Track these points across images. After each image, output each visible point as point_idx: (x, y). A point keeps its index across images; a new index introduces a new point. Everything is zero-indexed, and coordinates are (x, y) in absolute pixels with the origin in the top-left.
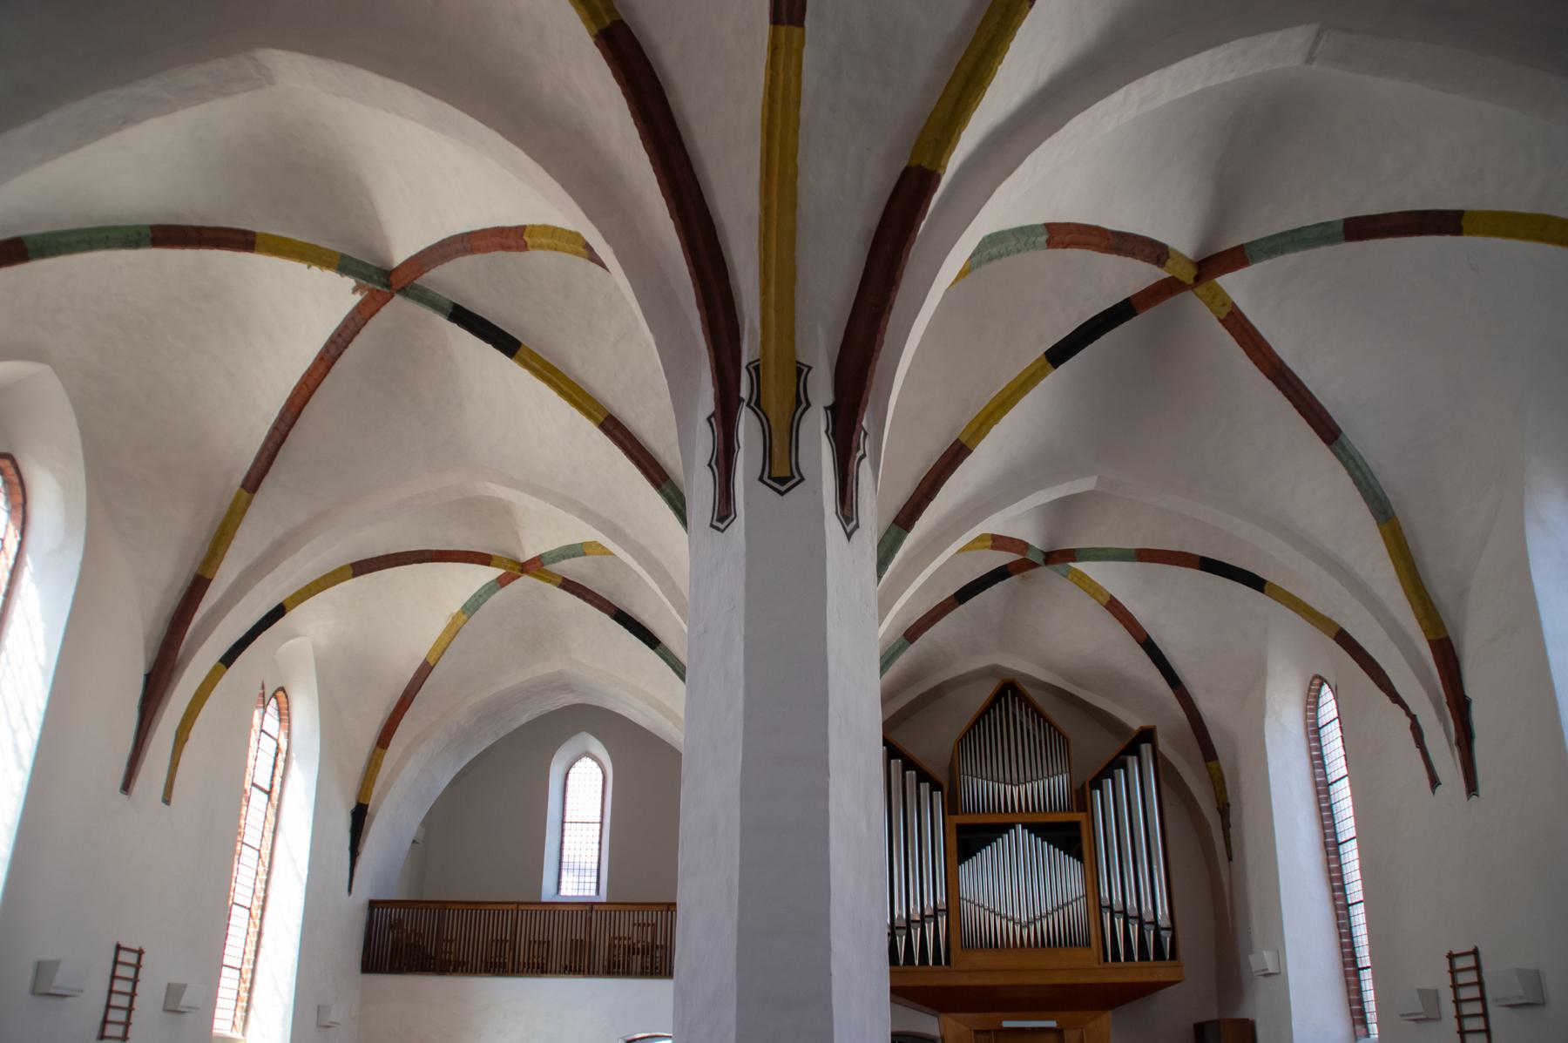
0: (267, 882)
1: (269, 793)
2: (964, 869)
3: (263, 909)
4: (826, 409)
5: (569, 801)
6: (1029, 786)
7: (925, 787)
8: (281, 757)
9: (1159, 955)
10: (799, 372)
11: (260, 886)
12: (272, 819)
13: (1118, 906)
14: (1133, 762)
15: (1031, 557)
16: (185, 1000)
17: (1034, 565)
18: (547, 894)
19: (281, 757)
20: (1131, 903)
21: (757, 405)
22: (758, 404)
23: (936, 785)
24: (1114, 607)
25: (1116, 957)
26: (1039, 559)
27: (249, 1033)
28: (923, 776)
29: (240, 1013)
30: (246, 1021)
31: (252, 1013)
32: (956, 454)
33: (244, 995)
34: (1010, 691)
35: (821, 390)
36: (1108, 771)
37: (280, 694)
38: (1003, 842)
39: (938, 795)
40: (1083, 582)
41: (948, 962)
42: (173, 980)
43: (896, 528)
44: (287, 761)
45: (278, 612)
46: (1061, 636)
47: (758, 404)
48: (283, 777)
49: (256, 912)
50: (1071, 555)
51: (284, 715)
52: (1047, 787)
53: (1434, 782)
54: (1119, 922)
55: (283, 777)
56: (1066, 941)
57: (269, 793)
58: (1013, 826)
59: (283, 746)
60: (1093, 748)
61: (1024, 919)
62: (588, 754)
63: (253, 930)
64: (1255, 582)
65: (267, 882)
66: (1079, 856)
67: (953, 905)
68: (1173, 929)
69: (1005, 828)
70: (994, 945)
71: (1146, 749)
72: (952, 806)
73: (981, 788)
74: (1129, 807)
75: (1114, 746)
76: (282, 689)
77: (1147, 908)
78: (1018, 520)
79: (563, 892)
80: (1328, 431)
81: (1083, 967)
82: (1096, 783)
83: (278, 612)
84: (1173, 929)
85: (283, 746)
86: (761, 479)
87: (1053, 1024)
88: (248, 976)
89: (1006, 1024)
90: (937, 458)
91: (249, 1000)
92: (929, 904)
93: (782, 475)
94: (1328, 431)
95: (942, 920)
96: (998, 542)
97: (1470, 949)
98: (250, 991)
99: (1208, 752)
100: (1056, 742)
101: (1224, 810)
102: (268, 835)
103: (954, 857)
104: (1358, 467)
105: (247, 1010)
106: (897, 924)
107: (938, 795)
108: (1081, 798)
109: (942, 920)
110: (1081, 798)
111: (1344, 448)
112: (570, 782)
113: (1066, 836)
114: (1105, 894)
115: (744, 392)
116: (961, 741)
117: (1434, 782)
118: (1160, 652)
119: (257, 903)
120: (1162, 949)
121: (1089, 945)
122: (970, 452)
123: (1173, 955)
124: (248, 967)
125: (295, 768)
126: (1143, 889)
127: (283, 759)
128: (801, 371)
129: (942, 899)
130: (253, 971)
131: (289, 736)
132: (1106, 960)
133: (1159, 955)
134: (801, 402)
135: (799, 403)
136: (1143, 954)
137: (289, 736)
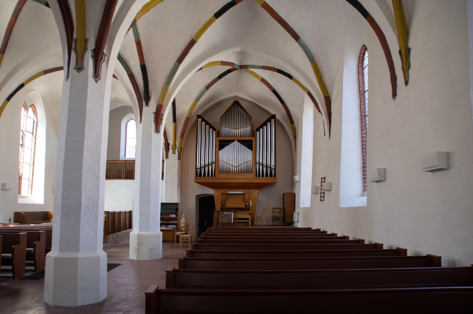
0: (34, 157)
1: (33, 133)
2: (220, 152)
3: (34, 164)
4: (92, 50)
5: (127, 130)
6: (238, 130)
7: (211, 130)
8: (35, 124)
9: (271, 175)
10: (86, 41)
11: (32, 158)
12: (34, 140)
13: (261, 163)
14: (269, 124)
15: (235, 67)
16: (7, 187)
17: (237, 69)
18: (122, 157)
19: (35, 124)
20: (265, 162)
21: (75, 50)
22: (76, 49)
23: (214, 129)
24: (263, 80)
25: (259, 176)
26: (238, 68)
27: (33, 194)
28: (211, 126)
29: (30, 191)
30: (31, 192)
31: (33, 190)
32: (192, 43)
33: (30, 186)
34: (236, 103)
35: (91, 45)
36: (262, 127)
37: (33, 106)
38: (231, 145)
39: (214, 132)
40: (253, 73)
41: (215, 176)
42: (3, 182)
43: (177, 63)
44: (37, 124)
45: (22, 86)
46: (251, 89)
47: (76, 49)
48: (36, 129)
49: (32, 165)
50: (246, 67)
51: (35, 112)
52: (244, 130)
53: (325, 135)
54: (261, 167)
55: (36, 129)
56: (247, 171)
57: (33, 133)
58: (234, 141)
59: (36, 121)
60: (259, 119)
61: (236, 165)
62: (132, 119)
63: (31, 170)
64: (290, 77)
65: (34, 157)
66: (252, 150)
67: (217, 161)
68: (275, 169)
69: (230, 142)
70: (228, 172)
71: (273, 120)
72: (218, 135)
73: (226, 130)
74: (267, 135)
75: (267, 117)
76: (33, 105)
77: (269, 163)
78: (229, 56)
79: (127, 157)
80: (296, 37)
81: (250, 178)
82: (258, 130)
83: (22, 86)
84: (275, 169)
85: (36, 121)
86: (79, 72)
87: (242, 193)
88: (31, 181)
89: (229, 192)
90: (187, 44)
91: (32, 187)
92: (210, 161)
93: (80, 68)
94: (296, 37)
95: (214, 165)
96: (223, 63)
97: (323, 177)
98: (32, 185)
99: (292, 122)
100: (248, 117)
101: (295, 137)
102: (33, 145)
103: (218, 148)
104: (305, 48)
105: (32, 190)
106: (202, 166)
107: (214, 132)
108: (253, 134)
109: (214, 165)
110: (253, 134)
111: (300, 42)
112: (128, 127)
113: (248, 144)
114: (258, 160)
115: (73, 47)
116: (222, 117)
117: (325, 135)
118: (278, 93)
119: (32, 163)
120: (272, 174)
121: (252, 172)
122: (196, 42)
123: (275, 176)
124: (31, 179)
125: (40, 126)
126: (267, 157)
127: (35, 124)
128: (86, 41)
129: (214, 160)
130: (32, 180)
131: (37, 118)
132: (256, 176)
133: (271, 175)
134: (85, 49)
135: (85, 49)
136: (263, 176)
137: (37, 118)
